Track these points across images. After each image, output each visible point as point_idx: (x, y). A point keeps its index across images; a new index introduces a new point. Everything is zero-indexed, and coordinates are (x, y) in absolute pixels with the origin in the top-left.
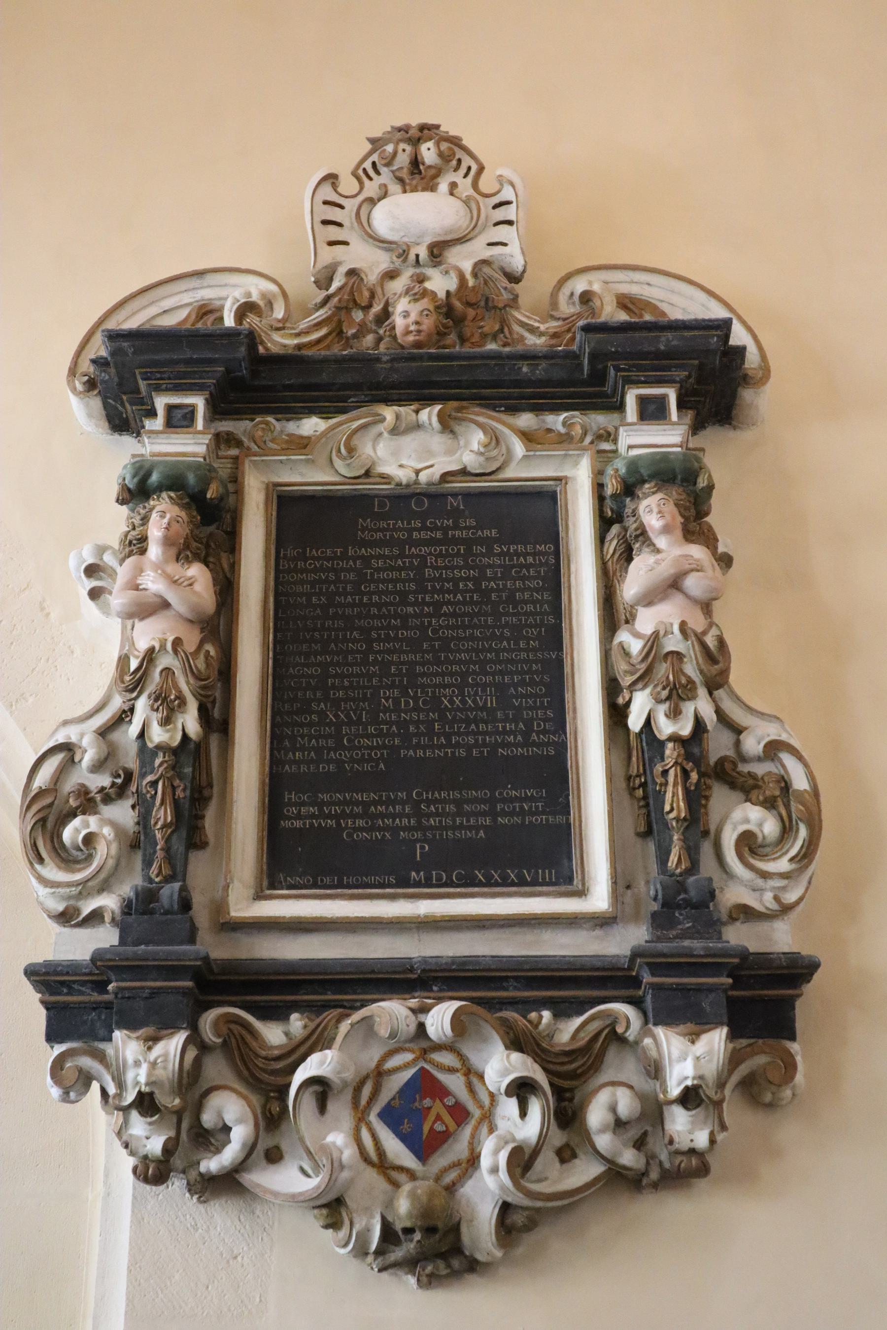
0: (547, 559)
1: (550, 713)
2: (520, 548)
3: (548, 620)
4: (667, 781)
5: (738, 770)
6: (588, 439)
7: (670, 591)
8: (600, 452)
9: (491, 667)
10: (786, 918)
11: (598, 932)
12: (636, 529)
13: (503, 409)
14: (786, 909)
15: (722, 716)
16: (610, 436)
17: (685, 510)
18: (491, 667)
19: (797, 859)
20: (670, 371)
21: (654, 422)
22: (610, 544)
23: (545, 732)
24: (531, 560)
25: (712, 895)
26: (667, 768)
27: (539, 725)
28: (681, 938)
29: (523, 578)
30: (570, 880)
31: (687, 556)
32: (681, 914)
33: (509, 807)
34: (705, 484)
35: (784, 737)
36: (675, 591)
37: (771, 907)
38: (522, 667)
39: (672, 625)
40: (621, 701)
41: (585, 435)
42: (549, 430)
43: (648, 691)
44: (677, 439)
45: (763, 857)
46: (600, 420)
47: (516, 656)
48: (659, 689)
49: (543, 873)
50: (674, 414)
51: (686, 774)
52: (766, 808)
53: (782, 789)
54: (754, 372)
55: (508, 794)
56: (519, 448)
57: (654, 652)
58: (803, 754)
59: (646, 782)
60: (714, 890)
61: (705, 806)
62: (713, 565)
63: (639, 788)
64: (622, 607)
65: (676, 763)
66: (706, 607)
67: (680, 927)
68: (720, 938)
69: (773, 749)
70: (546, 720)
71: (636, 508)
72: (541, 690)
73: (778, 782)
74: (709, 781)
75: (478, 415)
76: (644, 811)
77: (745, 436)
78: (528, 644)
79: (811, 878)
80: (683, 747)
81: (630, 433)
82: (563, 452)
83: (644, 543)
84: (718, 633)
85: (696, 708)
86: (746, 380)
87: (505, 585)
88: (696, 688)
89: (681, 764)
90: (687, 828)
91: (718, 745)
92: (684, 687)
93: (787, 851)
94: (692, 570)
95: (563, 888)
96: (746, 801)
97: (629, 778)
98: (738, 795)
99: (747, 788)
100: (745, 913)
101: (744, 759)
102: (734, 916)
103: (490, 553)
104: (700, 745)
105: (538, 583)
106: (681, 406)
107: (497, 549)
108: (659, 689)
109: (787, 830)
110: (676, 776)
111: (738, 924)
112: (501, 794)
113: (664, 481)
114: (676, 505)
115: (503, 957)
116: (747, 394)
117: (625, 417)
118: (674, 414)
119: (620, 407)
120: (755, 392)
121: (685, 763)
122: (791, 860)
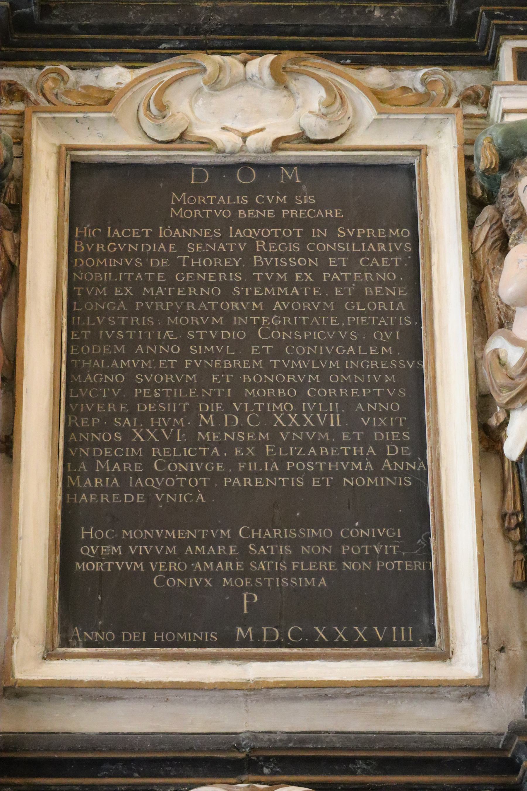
2: (369, 232)
6: (453, 101)
8: (466, 117)
9: (334, 378)
11: (465, 704)
12: (514, 213)
13: (349, 61)
16: (480, 98)
18: (334, 378)
23: (400, 458)
27: (393, 450)
29: (374, 270)
30: (431, 640)
33: (356, 550)
41: (449, 95)
42: (405, 89)
46: (465, 78)
49: (399, 631)
55: (355, 533)
56: (368, 109)
70: (401, 444)
71: (514, 187)
72: (395, 407)
78: (379, 350)
81: (506, 95)
82: (423, 117)
87: (351, 278)
97: (503, 517)
103: (332, 238)
105: (391, 276)
107: (341, 233)
112: (346, 533)
119: (491, 62)
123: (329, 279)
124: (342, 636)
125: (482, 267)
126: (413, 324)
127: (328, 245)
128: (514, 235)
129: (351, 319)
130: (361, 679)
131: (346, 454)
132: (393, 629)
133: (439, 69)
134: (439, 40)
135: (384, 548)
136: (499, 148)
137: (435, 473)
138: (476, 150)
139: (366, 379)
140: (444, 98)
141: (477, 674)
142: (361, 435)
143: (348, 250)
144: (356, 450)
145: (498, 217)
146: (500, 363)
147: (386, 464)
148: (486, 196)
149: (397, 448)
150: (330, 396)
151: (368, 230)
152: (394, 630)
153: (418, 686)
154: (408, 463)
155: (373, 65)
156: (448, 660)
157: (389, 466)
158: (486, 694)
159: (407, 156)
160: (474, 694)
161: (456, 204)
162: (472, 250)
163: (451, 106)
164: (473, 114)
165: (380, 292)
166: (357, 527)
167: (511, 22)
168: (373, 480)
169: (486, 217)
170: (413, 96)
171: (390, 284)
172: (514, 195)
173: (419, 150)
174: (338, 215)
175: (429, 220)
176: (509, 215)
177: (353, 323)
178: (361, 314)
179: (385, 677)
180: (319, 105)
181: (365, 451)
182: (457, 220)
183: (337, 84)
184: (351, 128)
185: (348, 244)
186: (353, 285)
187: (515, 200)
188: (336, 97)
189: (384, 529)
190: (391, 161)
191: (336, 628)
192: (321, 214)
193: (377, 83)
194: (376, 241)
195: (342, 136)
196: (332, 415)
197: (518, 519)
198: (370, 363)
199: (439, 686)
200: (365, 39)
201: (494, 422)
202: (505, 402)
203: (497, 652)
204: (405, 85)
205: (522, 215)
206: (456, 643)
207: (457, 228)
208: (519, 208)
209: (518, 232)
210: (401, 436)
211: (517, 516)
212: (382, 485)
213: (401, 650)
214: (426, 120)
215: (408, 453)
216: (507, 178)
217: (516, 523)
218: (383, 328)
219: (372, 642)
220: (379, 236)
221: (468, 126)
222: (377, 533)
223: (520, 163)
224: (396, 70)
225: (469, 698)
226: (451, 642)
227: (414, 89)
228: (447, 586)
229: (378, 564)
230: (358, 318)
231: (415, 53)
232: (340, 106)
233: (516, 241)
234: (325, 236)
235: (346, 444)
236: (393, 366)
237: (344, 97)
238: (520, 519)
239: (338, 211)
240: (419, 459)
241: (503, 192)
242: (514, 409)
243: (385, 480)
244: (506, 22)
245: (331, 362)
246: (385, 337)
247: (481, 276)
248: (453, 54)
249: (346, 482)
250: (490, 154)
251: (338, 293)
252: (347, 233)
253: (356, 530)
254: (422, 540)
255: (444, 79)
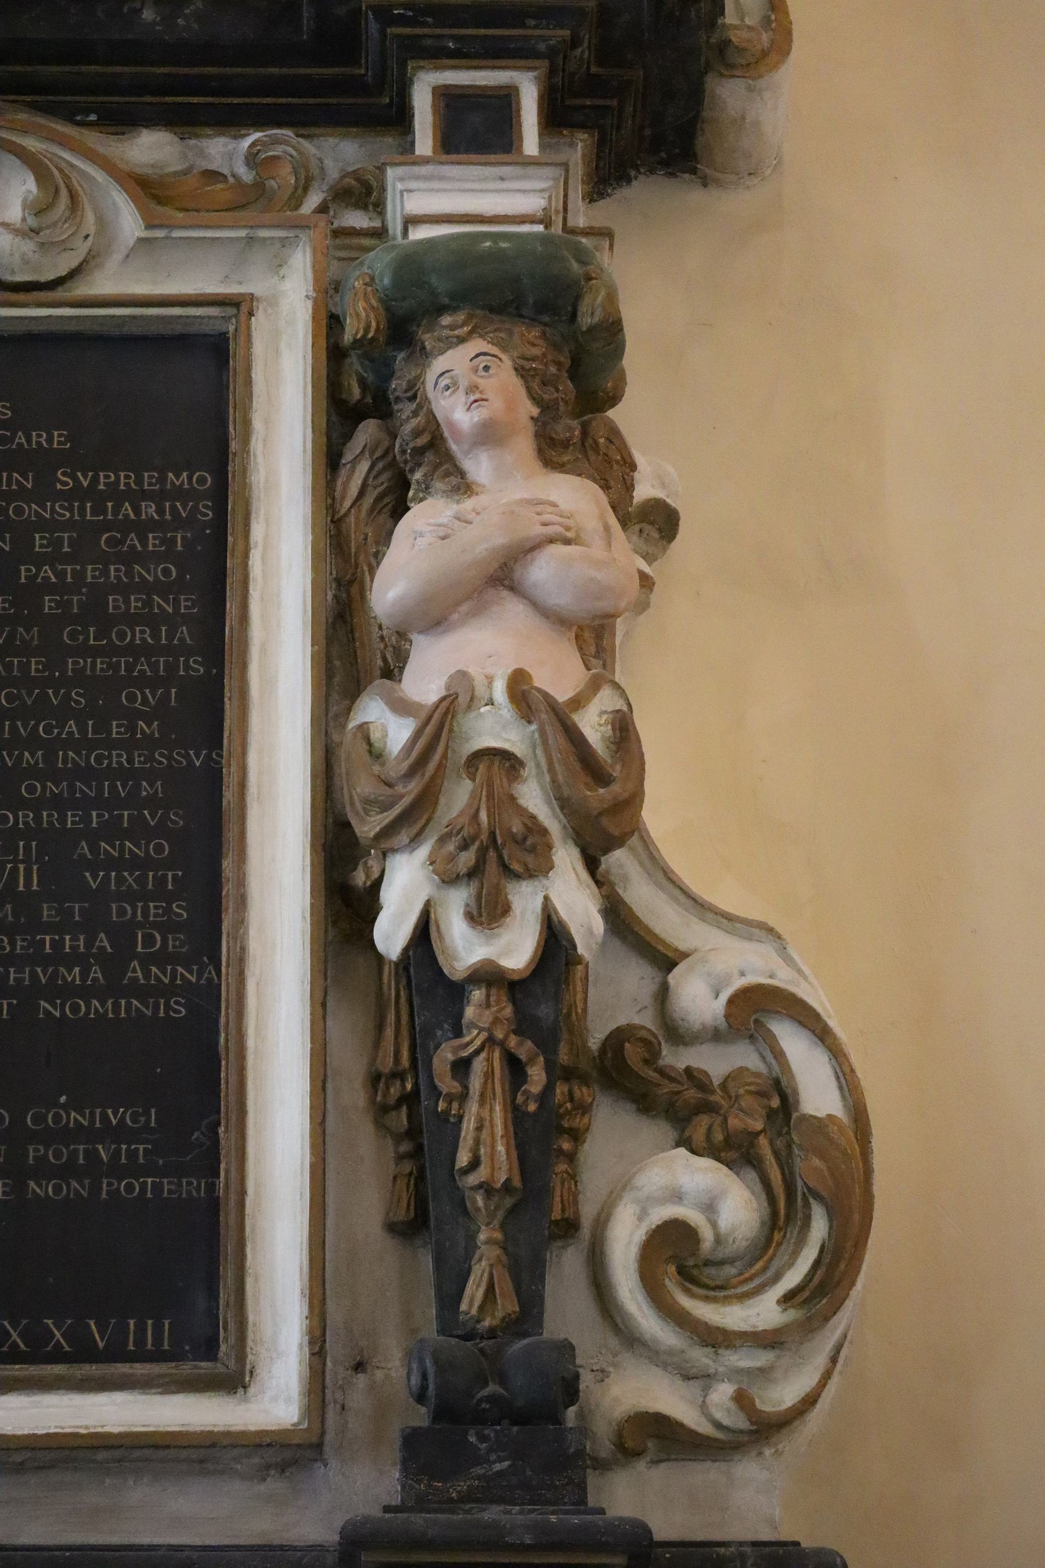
0: (195, 508)
1: (180, 911)
2: (125, 479)
3: (187, 667)
4: (466, 1088)
5: (661, 1062)
6: (313, 200)
7: (491, 591)
8: (339, 233)
9: (31, 789)
10: (768, 1452)
11: (274, 1485)
12: (417, 433)
13: (93, 117)
14: (764, 1429)
15: (618, 917)
16: (364, 192)
17: (544, 383)
18: (31, 789)
19: (799, 1298)
20: (523, 26)
21: (474, 157)
22: (353, 471)
23: (162, 958)
24: (152, 510)
25: (571, 1390)
26: (465, 1054)
27: (149, 940)
28: (477, 1501)
29: (131, 558)
30: (209, 1349)
31: (541, 503)
32: (483, 1438)
33: (58, 1155)
34: (596, 319)
35: (784, 978)
36: (505, 593)
37: (726, 1422)
38: (113, 788)
39: (490, 680)
40: (360, 878)
41: (306, 189)
42: (213, 176)
43: (423, 852)
44: (531, 203)
45: (717, 1291)
46: (339, 153)
47: (99, 759)
48: (451, 847)
49: (141, 1329)
50: (531, 141)
51: (516, 1068)
52: (729, 1164)
53: (771, 1115)
54: (744, 34)
55: (57, 1118)
56: (129, 222)
57: (440, 749)
58: (832, 1023)
59: (416, 1091)
60: (577, 1377)
61: (571, 1157)
62: (607, 528)
63: (397, 1106)
64: (375, 633)
65: (490, 1040)
66: (593, 636)
67: (479, 1471)
68: (583, 1501)
69: (755, 1008)
70: (165, 929)
71: (418, 378)
72: (159, 849)
73: (761, 1094)
74: (582, 1092)
75: (25, 132)
76: (407, 1167)
77: (733, 204)
78: (132, 728)
79: (838, 1349)
80: (513, 1000)
81: (413, 185)
82: (242, 233)
83: (436, 467)
84: (620, 705)
85: (546, 898)
86: (725, 57)
87: (79, 576)
88: (550, 847)
89: (502, 1044)
90: (512, 1211)
91: (613, 998)
92: (519, 842)
93: (777, 1278)
94: (551, 541)
95: (187, 1368)
96: (678, 1145)
97: (375, 1079)
98: (660, 1130)
99: (686, 1111)
100: (657, 1437)
101: (676, 1033)
102: (629, 1444)
103: (44, 492)
104: (557, 998)
105: (166, 572)
106: (554, 119)
107: (63, 480)
108: (451, 847)
109: (781, 1220)
110: (489, 1075)
111: (641, 1465)
112: (39, 1119)
113: (492, 310)
114: (521, 371)
115: (16, 1548)
116: (728, 93)
117: (413, 143)
118: (531, 141)
119: (399, 119)
120: (750, 89)
121: (513, 1041)
122: (788, 1299)
123: (31, 579)
124: (18, 1340)
125: (353, 550)
126: (208, 672)
127: (34, 506)
128: (418, 482)
129: (75, 663)
130: (44, 1432)
131: (48, 950)
132: (128, 1324)
133: (287, 133)
134: (285, 71)
135: (118, 1151)
136: (387, 296)
137: (233, 989)
138: (341, 300)
139: (100, 790)
140: (294, 193)
141: (295, 1420)
142: (81, 909)
143: (77, 518)
144: (71, 940)
145: (386, 444)
146: (370, 752)
147: (134, 971)
148: (369, 400)
149: (158, 937)
150: (21, 826)
151: (122, 474)
152: (132, 1327)
153: (168, 1447)
154: (180, 969)
155: (146, 127)
156: (241, 1390)
157: (140, 974)
158: (319, 1464)
159: (209, 317)
160: (295, 1462)
161: (305, 417)
162: (333, 515)
163: (309, 212)
164: (354, 228)
165: (140, 605)
166: (63, 1107)
167: (426, 31)
168: (103, 1004)
169: (363, 444)
170: (228, 189)
171: (163, 589)
172: (419, 396)
173: (239, 306)
174: (59, 443)
175: (248, 452)
176: (405, 438)
177: (79, 672)
178: (96, 652)
179: (95, 1427)
180: (24, 210)
181: (89, 945)
182: (305, 451)
183: (63, 165)
184: (94, 257)
185: (76, 504)
186: (84, 590)
187: (420, 407)
188: (57, 191)
189: (122, 1110)
190: (179, 329)
191: (6, 1323)
192: (23, 440)
193: (151, 162)
194: (137, 497)
195: (73, 274)
196: (21, 867)
197: (404, 1087)
198: (110, 757)
199: (213, 1445)
200: (127, 69)
201: (360, 878)
202: (372, 834)
203: (349, 1372)
204: (212, 167)
205: (434, 438)
206: (257, 1352)
207: (304, 469)
208: (428, 422)
209: (425, 475)
210: (168, 910)
211: (403, 1081)
212: (123, 1015)
213: (140, 1369)
214: (250, 240)
215: (181, 947)
216: (406, 360)
217: (398, 1094)
218: (142, 682)
219: (82, 1352)
220: (146, 487)
221: (342, 254)
222: (105, 1118)
223: (430, 329)
224: (197, 136)
225: (283, 1471)
226: (248, 1350)
227: (233, 176)
228: (248, 1230)
229: (104, 1186)
230: (89, 660)
231: (236, 101)
232: (67, 213)
233: (421, 495)
234: (29, 486)
235: (48, 928)
236: (161, 763)
237: (77, 192)
238: (409, 1086)
239: (59, 436)
240: (205, 959)
241: (395, 389)
242: (394, 851)
243: (129, 1005)
244: (418, 31)
245: (26, 754)
246: (145, 701)
247: (351, 571)
248: (318, 100)
249: (46, 1011)
250: (364, 309)
251: (50, 608)
252: (75, 479)
253: (62, 1112)
254: (202, 1133)
255: (294, 153)
